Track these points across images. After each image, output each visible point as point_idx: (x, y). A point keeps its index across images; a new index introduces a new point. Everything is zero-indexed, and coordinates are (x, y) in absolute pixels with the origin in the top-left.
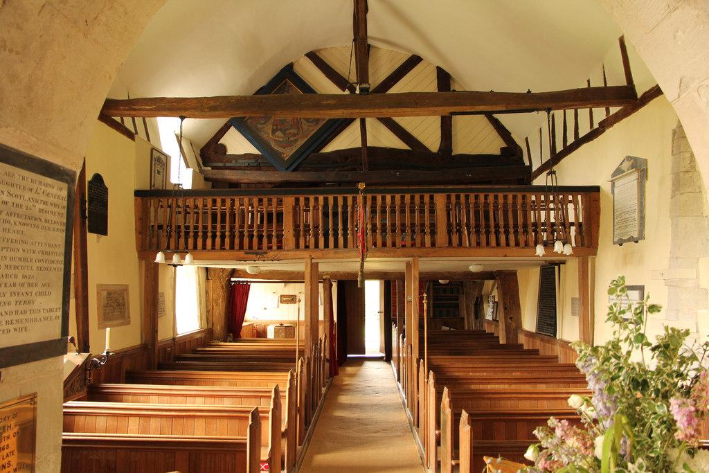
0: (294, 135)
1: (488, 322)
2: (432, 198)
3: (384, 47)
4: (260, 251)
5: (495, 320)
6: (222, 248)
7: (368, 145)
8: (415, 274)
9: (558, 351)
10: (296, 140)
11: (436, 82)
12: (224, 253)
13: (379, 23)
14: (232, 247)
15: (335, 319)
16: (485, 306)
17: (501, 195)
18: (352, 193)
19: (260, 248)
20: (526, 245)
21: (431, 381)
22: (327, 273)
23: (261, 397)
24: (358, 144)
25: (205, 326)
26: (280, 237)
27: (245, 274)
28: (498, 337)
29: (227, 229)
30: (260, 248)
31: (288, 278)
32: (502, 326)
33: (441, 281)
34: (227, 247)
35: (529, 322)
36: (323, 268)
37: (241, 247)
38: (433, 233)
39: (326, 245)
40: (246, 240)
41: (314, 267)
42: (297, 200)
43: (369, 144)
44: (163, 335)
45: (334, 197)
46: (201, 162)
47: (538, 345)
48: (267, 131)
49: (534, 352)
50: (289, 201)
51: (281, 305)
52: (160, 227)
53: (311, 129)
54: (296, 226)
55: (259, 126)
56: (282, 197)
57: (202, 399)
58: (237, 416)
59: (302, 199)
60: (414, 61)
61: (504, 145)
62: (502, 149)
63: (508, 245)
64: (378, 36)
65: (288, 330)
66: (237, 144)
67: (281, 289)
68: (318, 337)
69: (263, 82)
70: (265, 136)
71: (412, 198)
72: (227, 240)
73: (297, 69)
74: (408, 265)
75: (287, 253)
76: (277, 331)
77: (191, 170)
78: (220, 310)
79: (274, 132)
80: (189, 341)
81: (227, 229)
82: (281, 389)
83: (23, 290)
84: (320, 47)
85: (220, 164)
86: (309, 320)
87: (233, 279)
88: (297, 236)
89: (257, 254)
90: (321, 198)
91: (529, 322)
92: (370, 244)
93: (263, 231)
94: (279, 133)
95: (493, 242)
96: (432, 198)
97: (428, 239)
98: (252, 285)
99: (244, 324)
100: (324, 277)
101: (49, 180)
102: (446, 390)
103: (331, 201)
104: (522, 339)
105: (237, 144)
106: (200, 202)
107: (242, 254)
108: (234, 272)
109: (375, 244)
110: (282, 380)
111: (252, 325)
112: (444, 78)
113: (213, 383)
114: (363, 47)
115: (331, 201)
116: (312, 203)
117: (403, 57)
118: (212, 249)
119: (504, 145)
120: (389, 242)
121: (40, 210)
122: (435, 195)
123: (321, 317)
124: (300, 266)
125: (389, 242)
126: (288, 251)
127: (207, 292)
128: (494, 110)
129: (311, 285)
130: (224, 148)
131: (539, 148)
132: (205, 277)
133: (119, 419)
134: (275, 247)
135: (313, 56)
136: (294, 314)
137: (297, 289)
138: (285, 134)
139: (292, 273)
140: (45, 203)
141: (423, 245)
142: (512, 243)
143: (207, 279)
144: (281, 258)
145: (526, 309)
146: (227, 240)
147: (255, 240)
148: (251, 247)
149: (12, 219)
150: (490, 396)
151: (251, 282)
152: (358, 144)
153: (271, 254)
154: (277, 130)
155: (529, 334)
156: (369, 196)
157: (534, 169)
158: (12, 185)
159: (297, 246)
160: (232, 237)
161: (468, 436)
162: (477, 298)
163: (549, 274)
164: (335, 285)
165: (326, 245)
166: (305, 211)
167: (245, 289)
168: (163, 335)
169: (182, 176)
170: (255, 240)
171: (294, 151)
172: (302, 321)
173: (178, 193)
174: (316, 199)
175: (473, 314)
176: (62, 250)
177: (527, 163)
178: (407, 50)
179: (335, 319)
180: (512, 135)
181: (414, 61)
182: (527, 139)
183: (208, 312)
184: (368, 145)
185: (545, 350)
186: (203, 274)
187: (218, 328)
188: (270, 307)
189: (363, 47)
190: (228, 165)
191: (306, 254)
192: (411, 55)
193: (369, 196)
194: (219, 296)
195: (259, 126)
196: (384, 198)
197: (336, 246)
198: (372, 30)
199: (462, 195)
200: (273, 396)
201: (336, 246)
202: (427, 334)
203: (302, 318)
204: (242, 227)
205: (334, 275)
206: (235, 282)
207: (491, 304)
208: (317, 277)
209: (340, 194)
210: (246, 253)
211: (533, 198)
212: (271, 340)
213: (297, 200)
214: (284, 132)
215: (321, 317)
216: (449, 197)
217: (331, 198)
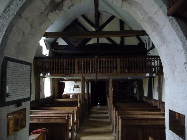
3: (104, 13)
5: (137, 93)
6: (58, 73)
8: (111, 80)
9: (153, 102)
12: (58, 74)
13: (102, 6)
15: (90, 92)
16: (134, 89)
17: (135, 58)
19: (68, 73)
20: (143, 72)
21: (114, 109)
22: (87, 79)
23: (69, 114)
24: (96, 42)
26: (74, 70)
27: (64, 80)
28: (137, 98)
29: (59, 67)
30: (68, 73)
31: (76, 81)
32: (138, 95)
33: (121, 82)
35: (146, 94)
36: (86, 78)
39: (87, 72)
40: (65, 71)
41: (84, 78)
42: (79, 60)
44: (41, 97)
46: (51, 47)
47: (148, 100)
49: (147, 102)
50: (76, 60)
51: (75, 89)
52: (41, 67)
54: (78, 67)
56: (82, 81)
57: (53, 114)
58: (64, 118)
59: (80, 60)
60: (113, 17)
61: (139, 42)
62: (139, 43)
63: (137, 72)
64: (102, 10)
65: (76, 96)
66: (61, 42)
67: (74, 84)
68: (85, 97)
71: (111, 59)
72: (59, 71)
73: (78, 20)
74: (110, 77)
76: (73, 96)
77: (48, 50)
78: (56, 90)
80: (48, 98)
81: (59, 67)
82: (74, 111)
83: (24, 88)
85: (57, 48)
86: (82, 93)
88: (79, 70)
89: (67, 75)
90: (85, 59)
91: (146, 94)
92: (99, 72)
95: (133, 72)
96: (116, 59)
97: (115, 71)
98: (66, 83)
99: (63, 94)
100: (87, 80)
101: (28, 66)
102: (117, 111)
103: (88, 60)
104: (144, 99)
105: (61, 42)
106: (52, 60)
107: (63, 75)
108: (61, 79)
109: (100, 72)
110: (75, 109)
111: (66, 94)
112: (122, 23)
113: (55, 110)
114: (98, 14)
115: (88, 60)
116: (83, 61)
117: (110, 16)
119: (139, 42)
120: (104, 72)
121: (27, 72)
123: (86, 92)
124: (80, 78)
125: (104, 72)
127: (53, 85)
130: (57, 43)
133: (32, 119)
135: (84, 16)
136: (78, 91)
139: (78, 79)
140: (27, 70)
141: (114, 72)
142: (139, 72)
146: (59, 71)
147: (67, 71)
148: (66, 73)
149: (23, 74)
150: (130, 114)
152: (96, 42)
153: (72, 75)
155: (146, 97)
156: (99, 59)
157: (148, 49)
158: (22, 68)
159: (79, 73)
160: (61, 70)
161: (120, 122)
163: (151, 79)
164: (90, 83)
165: (87, 72)
166: (81, 62)
167: (64, 84)
168: (41, 97)
169: (46, 52)
170: (67, 71)
173: (45, 57)
174: (84, 60)
176: (30, 79)
177: (146, 48)
178: (111, 14)
179: (90, 92)
181: (113, 17)
182: (146, 40)
185: (150, 102)
186: (52, 80)
187: (56, 95)
188: (70, 89)
189: (98, 14)
190: (59, 48)
191: (81, 75)
192: (111, 15)
193: (99, 59)
194: (56, 86)
196: (103, 59)
197: (89, 72)
198: (100, 9)
199: (125, 58)
200: (72, 113)
201: (89, 72)
203: (80, 92)
204: (63, 67)
205: (89, 80)
208: (84, 80)
211: (148, 59)
212: (71, 99)
213: (79, 60)
215: (86, 92)
216: (121, 59)
217: (88, 59)
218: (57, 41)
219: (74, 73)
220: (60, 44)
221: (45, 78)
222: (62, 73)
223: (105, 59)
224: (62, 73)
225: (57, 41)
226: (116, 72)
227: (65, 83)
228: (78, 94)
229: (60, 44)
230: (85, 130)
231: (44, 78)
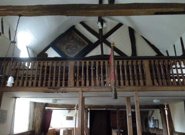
0: (75, 50)
1: (152, 128)
2: (142, 62)
4: (56, 87)
7: (104, 54)
10: (75, 52)
11: (128, 32)
12: (38, 88)
14: (42, 85)
16: (149, 122)
18: (103, 60)
24: (100, 53)
25: (31, 129)
31: (70, 108)
34: (39, 85)
37: (46, 85)
38: (144, 79)
39: (90, 85)
40: (49, 82)
43: (104, 54)
45: (94, 62)
48: (64, 48)
53: (81, 48)
55: (61, 47)
56: (100, 61)
69: (63, 31)
70: (63, 50)
73: (76, 27)
75: (70, 88)
79: (67, 49)
84: (85, 21)
86: (80, 127)
87: (46, 108)
89: (54, 89)
93: (58, 78)
94: (69, 49)
96: (142, 62)
97: (141, 82)
98: (53, 111)
99: (49, 129)
105: (52, 53)
111: (54, 129)
118: (31, 86)
122: (143, 61)
126: (70, 87)
127: (34, 113)
128: (178, 11)
129: (82, 105)
130: (47, 55)
131: (176, 51)
132: (34, 107)
134: (63, 85)
136: (71, 124)
137: (74, 113)
138: (71, 50)
143: (35, 107)
144: (67, 91)
145: (175, 121)
151: (53, 109)
153: (62, 89)
154: (68, 48)
159: (75, 85)
162: (146, 118)
165: (90, 85)
167: (50, 112)
171: (75, 55)
172: (77, 128)
175: (144, 125)
180: (160, 51)
183: (33, 122)
184: (104, 54)
191: (79, 89)
192: (118, 23)
195: (61, 47)
202: (128, 133)
203: (77, 126)
206: (47, 109)
207: (152, 121)
209: (97, 60)
210: (49, 88)
214: (70, 49)
216: (150, 62)
218: (46, 52)
219: (66, 85)
220: (49, 56)
221: (17, 99)
222: (44, 85)
223: (123, 62)
224: (44, 85)
225: (46, 52)
226: (145, 84)
227: (52, 111)
228: (73, 129)
229: (49, 56)
230: (65, 129)
231: (16, 98)
